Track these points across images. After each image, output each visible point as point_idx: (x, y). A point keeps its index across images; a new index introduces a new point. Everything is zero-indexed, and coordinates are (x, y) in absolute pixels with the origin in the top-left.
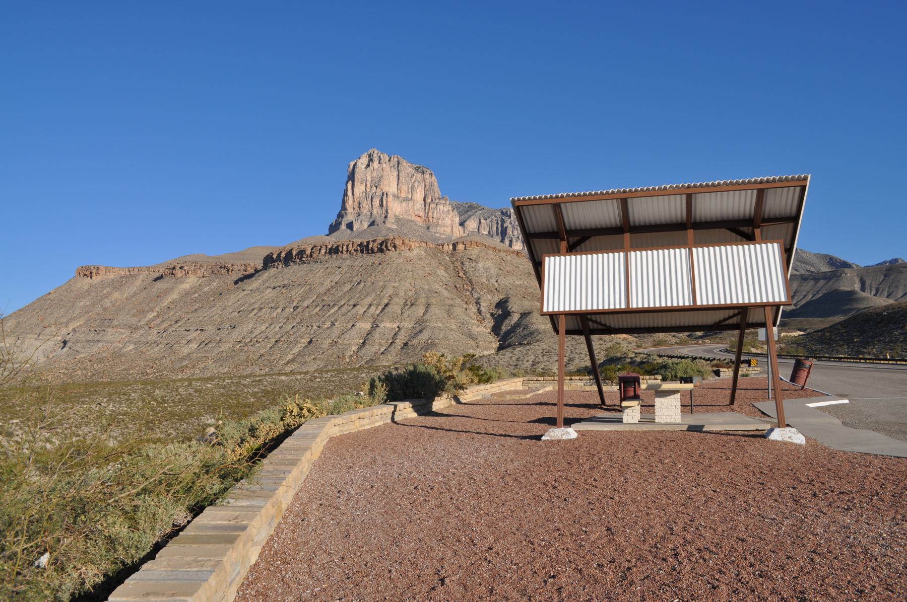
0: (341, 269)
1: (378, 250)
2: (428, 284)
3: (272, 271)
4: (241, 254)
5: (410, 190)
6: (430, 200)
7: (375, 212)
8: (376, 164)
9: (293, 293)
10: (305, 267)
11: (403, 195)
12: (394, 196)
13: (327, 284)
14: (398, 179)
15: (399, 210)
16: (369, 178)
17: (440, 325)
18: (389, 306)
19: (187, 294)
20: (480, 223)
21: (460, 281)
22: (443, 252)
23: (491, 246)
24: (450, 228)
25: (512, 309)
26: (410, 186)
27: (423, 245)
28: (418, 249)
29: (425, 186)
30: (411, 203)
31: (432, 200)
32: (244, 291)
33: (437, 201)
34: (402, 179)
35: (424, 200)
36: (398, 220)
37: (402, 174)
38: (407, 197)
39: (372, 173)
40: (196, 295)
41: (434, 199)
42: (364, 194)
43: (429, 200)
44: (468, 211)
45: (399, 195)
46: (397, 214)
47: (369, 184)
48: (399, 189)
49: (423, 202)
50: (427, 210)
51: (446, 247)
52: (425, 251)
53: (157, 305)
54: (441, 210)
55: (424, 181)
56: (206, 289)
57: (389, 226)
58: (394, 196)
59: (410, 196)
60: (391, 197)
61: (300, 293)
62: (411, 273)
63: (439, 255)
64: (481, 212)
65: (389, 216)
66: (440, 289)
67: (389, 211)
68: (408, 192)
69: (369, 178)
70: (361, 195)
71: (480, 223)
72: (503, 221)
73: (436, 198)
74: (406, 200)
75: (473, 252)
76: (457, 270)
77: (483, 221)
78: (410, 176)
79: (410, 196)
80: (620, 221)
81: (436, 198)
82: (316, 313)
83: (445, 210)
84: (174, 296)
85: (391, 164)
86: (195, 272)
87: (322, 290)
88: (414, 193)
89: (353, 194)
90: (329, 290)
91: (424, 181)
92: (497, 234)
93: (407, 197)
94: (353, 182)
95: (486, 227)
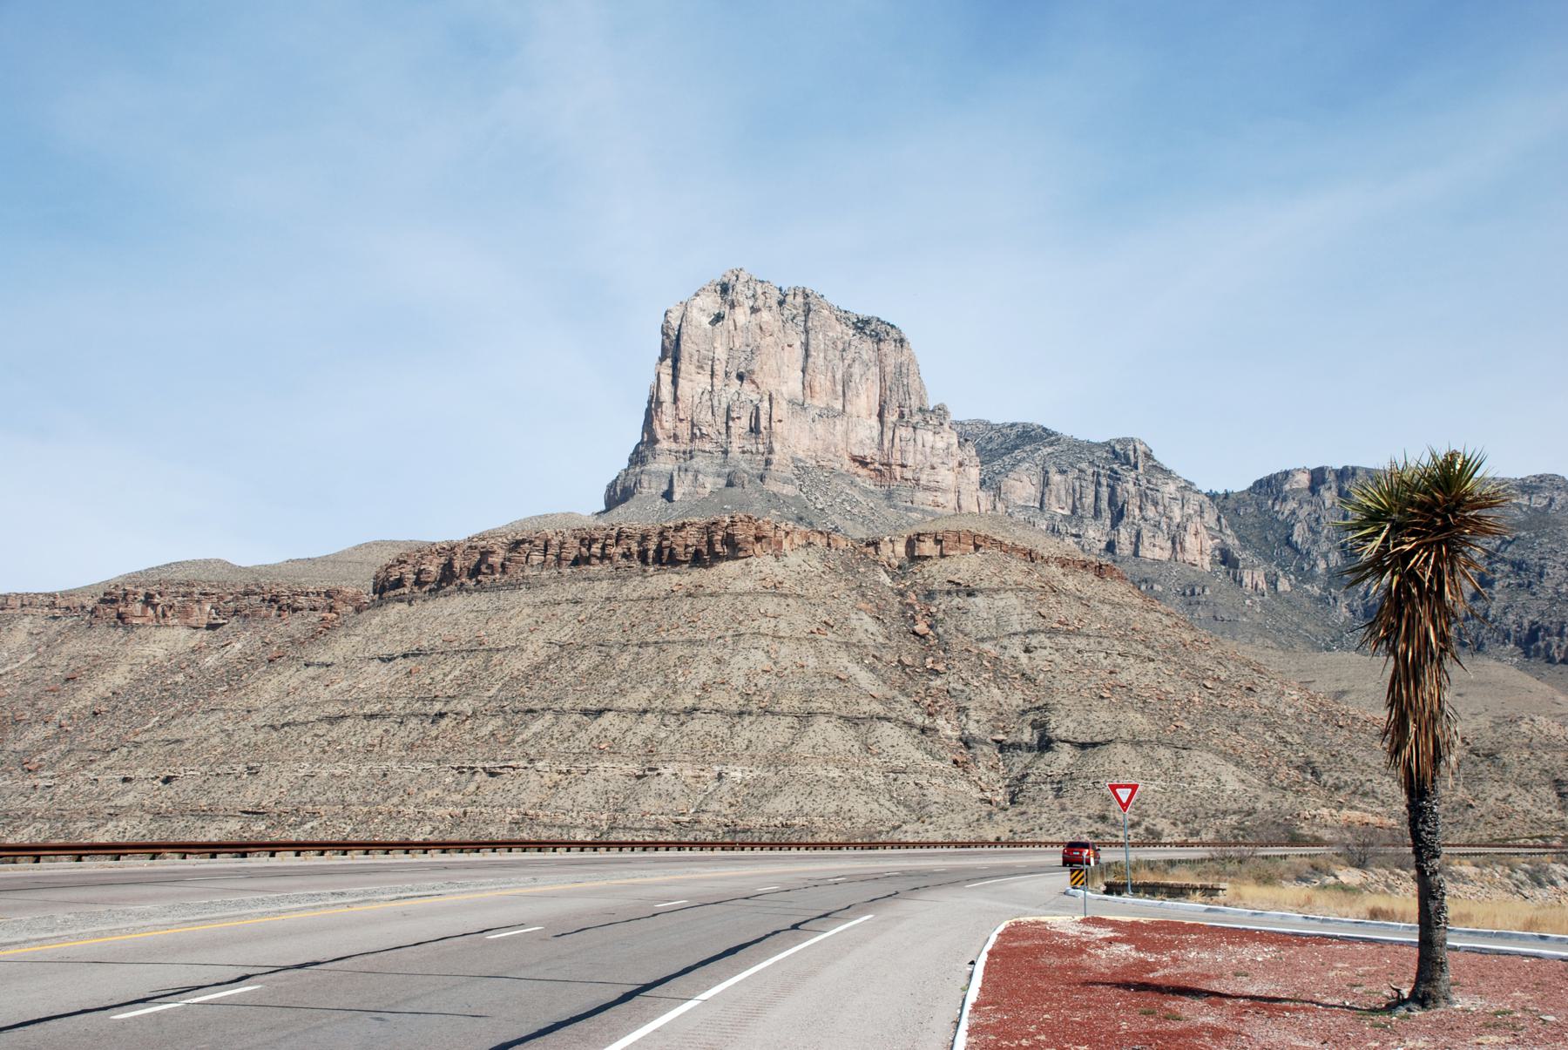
0: (579, 608)
1: (909, 562)
2: (820, 654)
3: (395, 611)
4: (334, 562)
5: (839, 388)
6: (895, 418)
7: (735, 448)
8: (741, 315)
9: (437, 673)
10: (481, 601)
11: (820, 401)
12: (791, 402)
13: (536, 648)
14: (807, 356)
15: (806, 441)
16: (721, 353)
17: (835, 773)
18: (1112, 745)
19: (157, 671)
20: (1046, 483)
21: (916, 647)
22: (876, 562)
23: (1021, 545)
24: (952, 497)
25: (1058, 731)
26: (839, 376)
27: (820, 541)
28: (802, 553)
29: (883, 379)
30: (840, 426)
31: (902, 416)
32: (307, 665)
33: (917, 418)
34: (817, 358)
35: (881, 415)
36: (801, 470)
37: (817, 341)
38: (829, 408)
39: (731, 337)
40: (180, 678)
41: (906, 411)
42: (706, 396)
43: (891, 417)
44: (1016, 447)
45: (808, 401)
46: (801, 455)
47: (720, 369)
48: (807, 386)
49: (874, 421)
50: (886, 444)
51: (885, 550)
52: (824, 558)
53: (61, 705)
54: (928, 445)
55: (880, 362)
56: (210, 661)
57: (775, 490)
58: (791, 402)
59: (838, 406)
60: (784, 405)
61: (457, 673)
62: (773, 622)
63: (862, 570)
64: (1050, 450)
65: (775, 458)
66: (854, 669)
67: (777, 446)
68: (834, 392)
69: (721, 353)
70: (697, 400)
71: (1046, 483)
72: (1115, 477)
73: (915, 409)
74: (828, 414)
75: (963, 566)
76: (910, 613)
77: (1056, 478)
78: (840, 347)
79: (838, 406)
80: (1483, 481)
81: (915, 409)
82: (493, 734)
83: (941, 445)
84: (119, 677)
85: (786, 312)
86: (185, 613)
87: (518, 664)
88: (849, 394)
89: (676, 399)
90: (537, 668)
91: (880, 362)
92: (1097, 513)
93: (829, 408)
94: (676, 361)
95: (1063, 492)
